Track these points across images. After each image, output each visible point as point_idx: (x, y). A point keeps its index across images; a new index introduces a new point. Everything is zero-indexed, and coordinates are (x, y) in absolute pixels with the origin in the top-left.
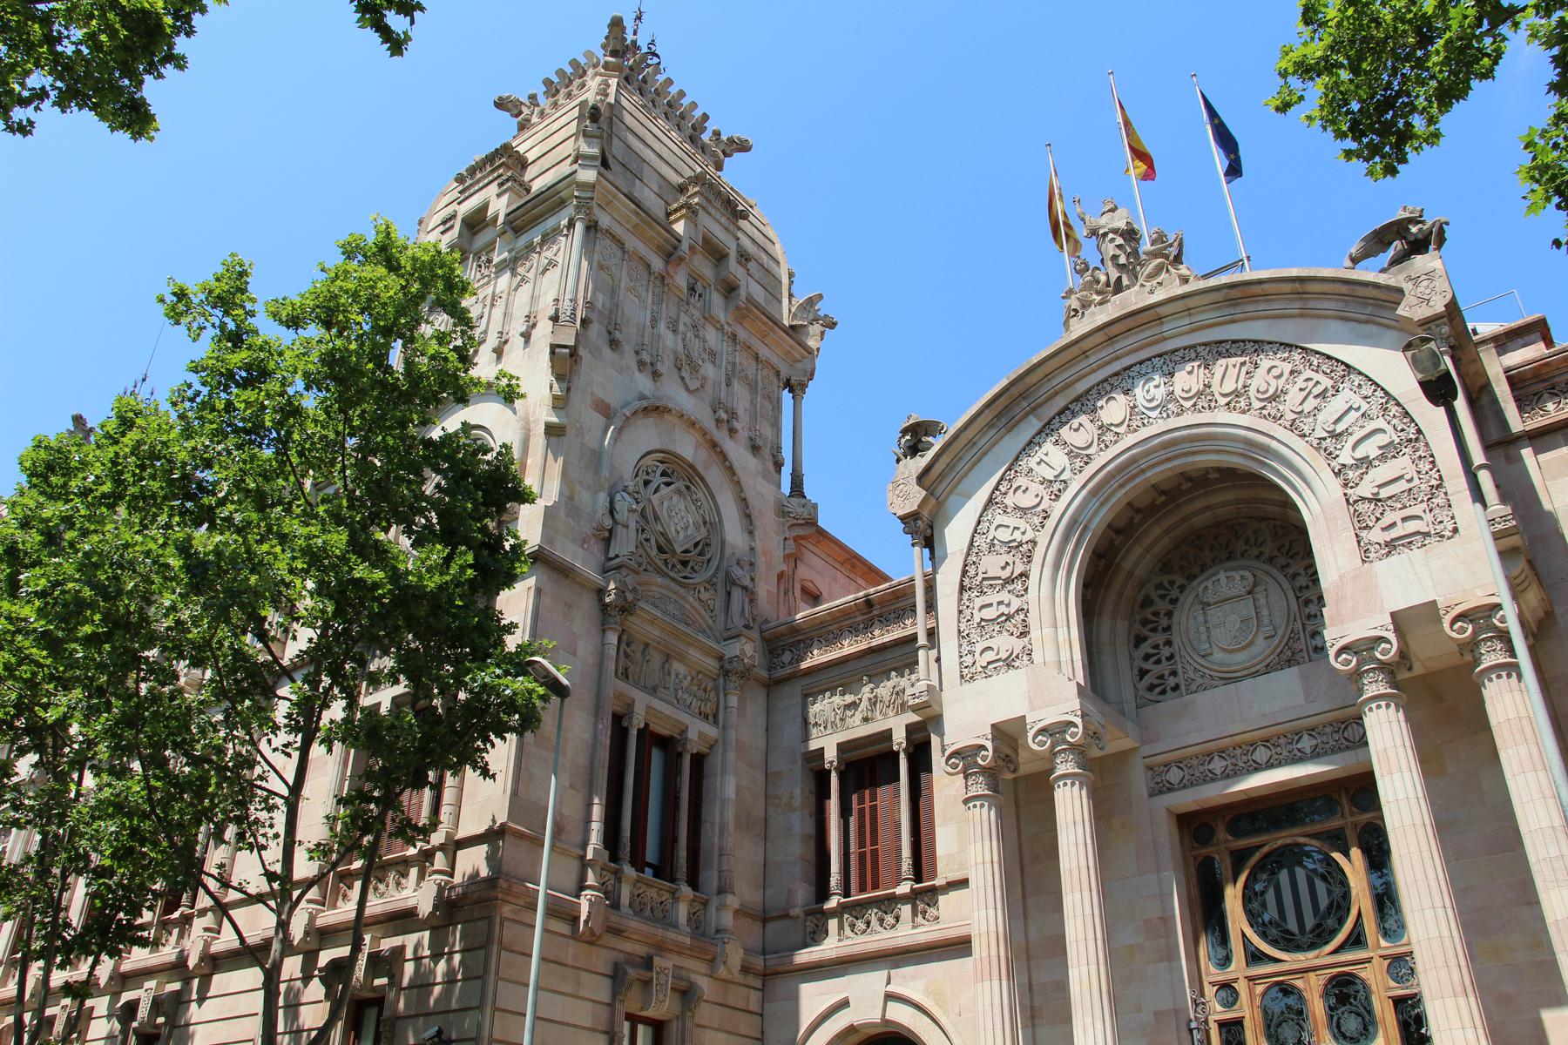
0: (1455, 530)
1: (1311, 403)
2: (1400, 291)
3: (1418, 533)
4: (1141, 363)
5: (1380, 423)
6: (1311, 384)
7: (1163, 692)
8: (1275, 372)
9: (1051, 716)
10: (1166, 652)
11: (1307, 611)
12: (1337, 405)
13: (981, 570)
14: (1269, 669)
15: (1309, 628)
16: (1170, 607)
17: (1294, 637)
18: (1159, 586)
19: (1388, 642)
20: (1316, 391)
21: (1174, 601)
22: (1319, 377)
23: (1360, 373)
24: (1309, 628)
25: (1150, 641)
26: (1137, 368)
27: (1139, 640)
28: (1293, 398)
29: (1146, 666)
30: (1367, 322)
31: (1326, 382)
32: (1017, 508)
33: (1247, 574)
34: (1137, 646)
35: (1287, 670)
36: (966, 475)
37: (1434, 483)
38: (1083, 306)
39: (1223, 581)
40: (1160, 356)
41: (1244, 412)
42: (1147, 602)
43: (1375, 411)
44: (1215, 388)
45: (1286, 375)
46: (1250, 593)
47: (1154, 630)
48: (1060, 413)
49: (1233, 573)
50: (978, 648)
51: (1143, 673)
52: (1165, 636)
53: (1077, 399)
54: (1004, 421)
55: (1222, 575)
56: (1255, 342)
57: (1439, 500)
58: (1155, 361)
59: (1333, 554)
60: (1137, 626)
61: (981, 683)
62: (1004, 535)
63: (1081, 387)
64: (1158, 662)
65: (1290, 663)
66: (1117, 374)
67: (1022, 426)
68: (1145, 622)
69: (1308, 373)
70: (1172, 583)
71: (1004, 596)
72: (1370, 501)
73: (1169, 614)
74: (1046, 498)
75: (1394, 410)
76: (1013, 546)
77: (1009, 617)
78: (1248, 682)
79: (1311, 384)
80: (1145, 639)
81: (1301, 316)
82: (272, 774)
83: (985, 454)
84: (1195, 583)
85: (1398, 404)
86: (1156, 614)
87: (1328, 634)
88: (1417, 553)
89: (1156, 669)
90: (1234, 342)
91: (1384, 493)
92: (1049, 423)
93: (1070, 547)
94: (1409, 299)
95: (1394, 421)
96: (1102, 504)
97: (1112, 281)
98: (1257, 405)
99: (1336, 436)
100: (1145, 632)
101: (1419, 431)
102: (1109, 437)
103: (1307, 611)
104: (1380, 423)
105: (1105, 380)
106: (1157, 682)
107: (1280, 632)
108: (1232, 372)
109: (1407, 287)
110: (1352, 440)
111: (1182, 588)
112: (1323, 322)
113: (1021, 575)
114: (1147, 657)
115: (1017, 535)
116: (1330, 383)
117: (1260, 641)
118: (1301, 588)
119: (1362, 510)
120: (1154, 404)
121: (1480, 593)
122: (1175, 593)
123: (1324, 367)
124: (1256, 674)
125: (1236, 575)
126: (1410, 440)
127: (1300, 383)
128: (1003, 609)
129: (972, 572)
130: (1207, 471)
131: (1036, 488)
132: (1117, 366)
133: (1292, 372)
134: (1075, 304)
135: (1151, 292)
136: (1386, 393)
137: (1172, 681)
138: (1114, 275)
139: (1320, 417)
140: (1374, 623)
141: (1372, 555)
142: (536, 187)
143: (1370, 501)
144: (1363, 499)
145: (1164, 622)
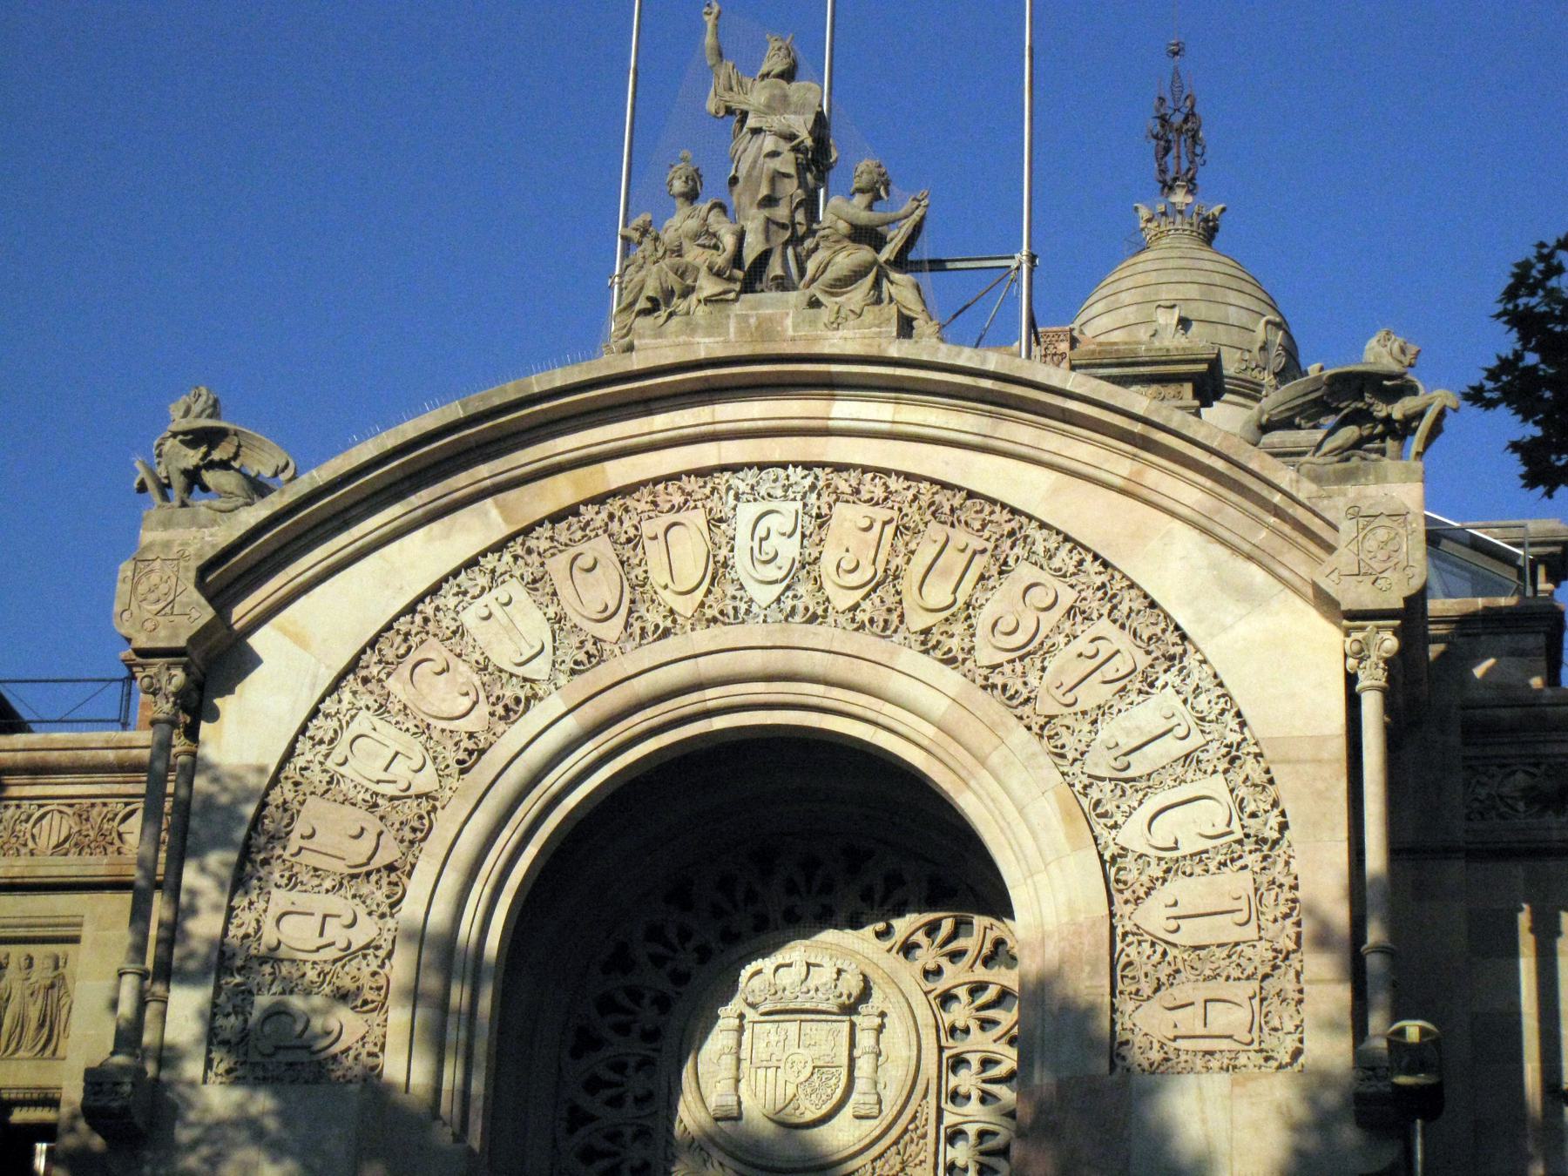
1: (1090, 696)
4: (762, 466)
8: (1040, 597)
11: (953, 1081)
12: (1147, 715)
15: (949, 1119)
16: (667, 987)
20: (1109, 671)
22: (1122, 640)
24: (949, 1119)
27: (586, 1042)
28: (1064, 663)
29: (586, 1102)
30: (1250, 558)
34: (576, 1054)
40: (808, 466)
44: (909, 584)
47: (622, 1029)
48: (556, 518)
51: (578, 1118)
63: (618, 473)
64: (616, 1102)
66: (703, 473)
68: (607, 1005)
69: (1104, 626)
70: (685, 935)
73: (663, 1003)
80: (597, 1044)
86: (635, 995)
89: (609, 1117)
90: (971, 495)
92: (527, 531)
93: (508, 837)
97: (749, 256)
99: (1124, 782)
103: (953, 1081)
104: (1217, 786)
105: (676, 477)
108: (954, 560)
113: (391, 868)
114: (593, 1085)
116: (1143, 661)
118: (953, 1031)
120: (772, 572)
123: (1135, 622)
127: (1082, 644)
133: (1070, 612)
135: (836, 324)
139: (1109, 730)
142: (237, 627)
145: (648, 1015)
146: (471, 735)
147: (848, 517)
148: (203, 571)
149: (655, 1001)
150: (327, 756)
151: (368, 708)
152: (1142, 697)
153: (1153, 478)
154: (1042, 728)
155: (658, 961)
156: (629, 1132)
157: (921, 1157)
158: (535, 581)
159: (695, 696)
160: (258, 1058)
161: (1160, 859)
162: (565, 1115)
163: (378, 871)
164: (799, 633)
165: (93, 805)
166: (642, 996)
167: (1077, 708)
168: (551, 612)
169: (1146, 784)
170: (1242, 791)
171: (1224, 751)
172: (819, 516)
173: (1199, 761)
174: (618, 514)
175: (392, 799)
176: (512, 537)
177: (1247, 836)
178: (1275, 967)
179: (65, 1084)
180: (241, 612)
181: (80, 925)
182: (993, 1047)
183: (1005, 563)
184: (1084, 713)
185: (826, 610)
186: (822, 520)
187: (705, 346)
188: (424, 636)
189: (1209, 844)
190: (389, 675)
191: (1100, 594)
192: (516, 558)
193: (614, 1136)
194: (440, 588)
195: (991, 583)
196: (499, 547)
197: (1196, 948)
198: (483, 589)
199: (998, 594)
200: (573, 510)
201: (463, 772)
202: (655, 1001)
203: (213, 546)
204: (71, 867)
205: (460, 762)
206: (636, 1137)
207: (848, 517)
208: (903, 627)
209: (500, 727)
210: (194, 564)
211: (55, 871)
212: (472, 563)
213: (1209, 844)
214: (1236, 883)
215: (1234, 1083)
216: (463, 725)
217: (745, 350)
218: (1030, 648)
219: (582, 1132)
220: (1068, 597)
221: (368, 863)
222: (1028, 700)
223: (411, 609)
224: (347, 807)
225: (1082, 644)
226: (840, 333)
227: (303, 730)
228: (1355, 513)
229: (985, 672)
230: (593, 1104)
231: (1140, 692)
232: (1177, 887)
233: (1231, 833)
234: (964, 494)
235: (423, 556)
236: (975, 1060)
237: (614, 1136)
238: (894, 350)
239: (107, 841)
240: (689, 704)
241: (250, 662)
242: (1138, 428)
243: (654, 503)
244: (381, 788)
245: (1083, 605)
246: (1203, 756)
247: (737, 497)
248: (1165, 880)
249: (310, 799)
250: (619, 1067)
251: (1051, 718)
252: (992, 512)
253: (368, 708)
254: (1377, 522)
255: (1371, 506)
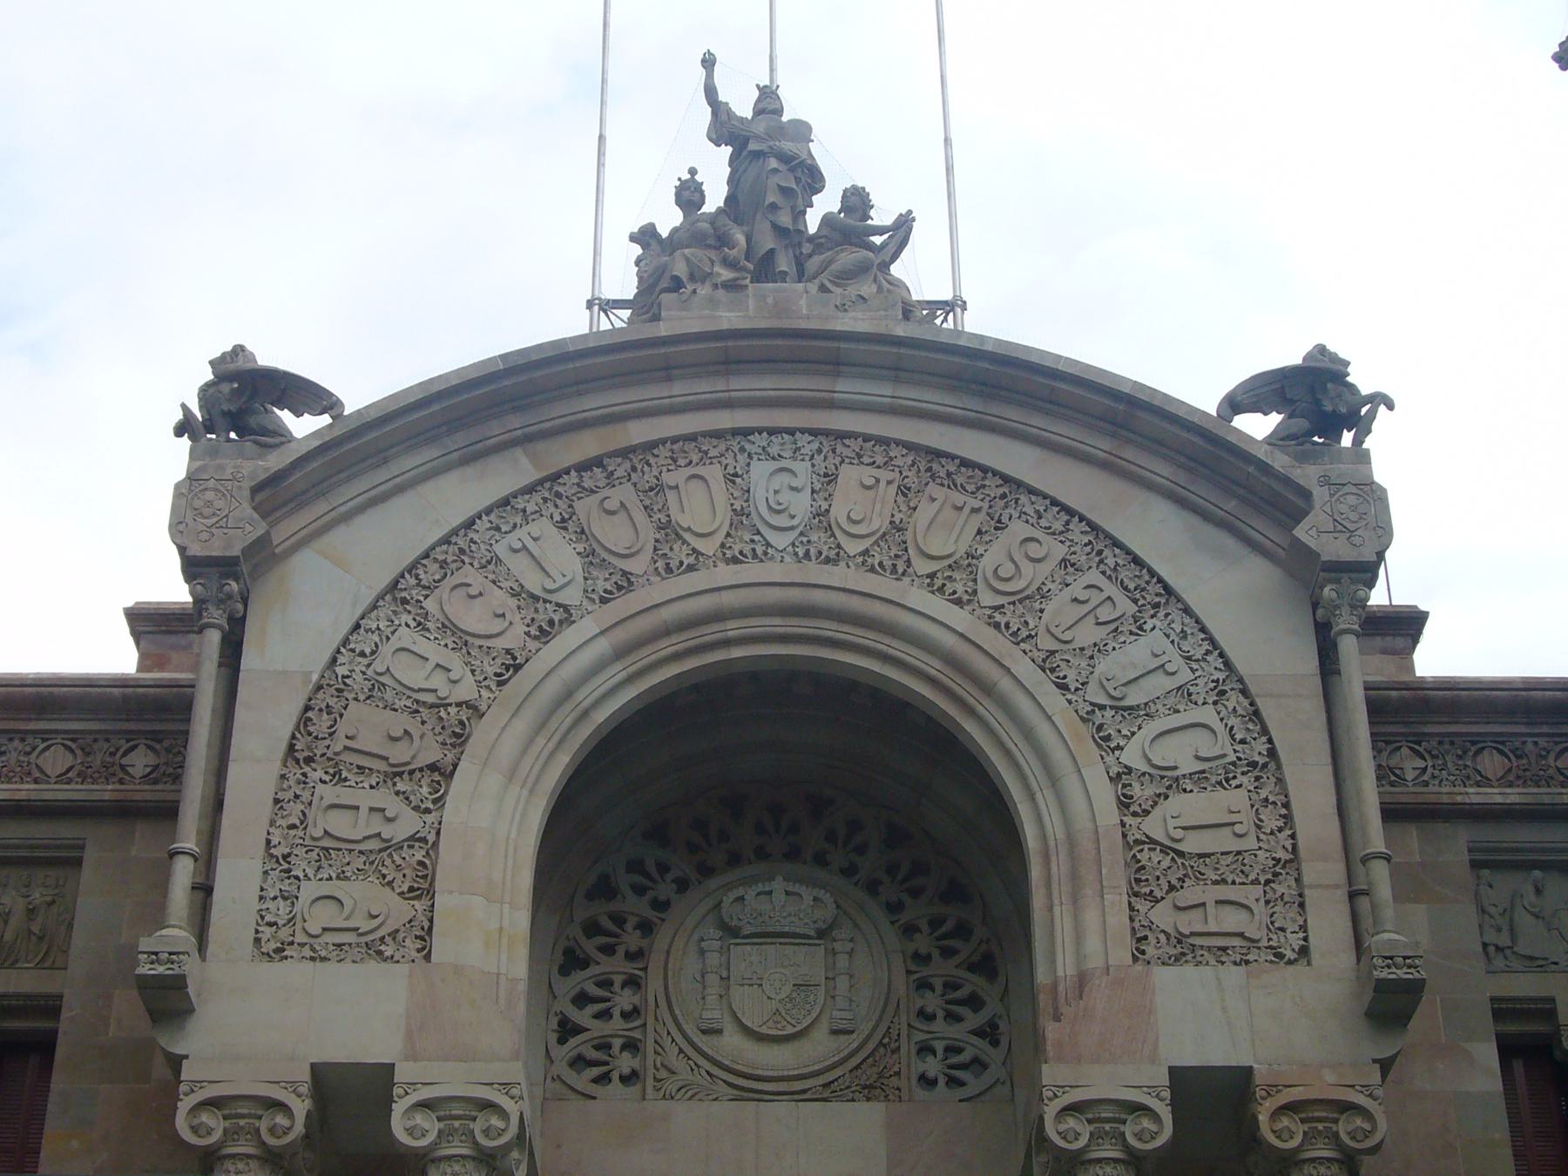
0: (1304, 951)
1: (1087, 634)
2: (1306, 495)
3: (1241, 935)
4: (773, 432)
5: (1207, 715)
6: (1096, 597)
7: (603, 1079)
9: (453, 1081)
10: (625, 999)
12: (1138, 653)
13: (343, 728)
14: (829, 1092)
16: (650, 914)
17: (888, 1045)
18: (635, 866)
19: (1156, 1117)
20: (1105, 613)
21: (661, 906)
22: (1111, 590)
23: (1187, 610)
25: (593, 970)
26: (760, 440)
28: (1059, 610)
31: (1125, 606)
32: (448, 626)
33: (827, 898)
35: (863, 1107)
36: (347, 517)
37: (1281, 854)
38: (692, 278)
39: (779, 897)
40: (814, 433)
41: (958, 602)
42: (604, 889)
43: (1201, 690)
45: (1051, 564)
46: (821, 934)
47: (609, 950)
48: (583, 467)
49: (802, 889)
50: (308, 891)
51: (567, 1030)
52: (631, 968)
53: (625, 453)
54: (460, 439)
55: (778, 885)
56: (1006, 479)
57: (1285, 887)
58: (803, 439)
59: (1078, 931)
60: (576, 931)
61: (296, 971)
62: (414, 675)
63: (639, 432)
64: (605, 1015)
65: (870, 1091)
66: (718, 435)
67: (495, 462)
68: (592, 929)
69: (1094, 576)
70: (663, 868)
71: (384, 798)
72: (1165, 850)
73: (646, 928)
74: (520, 629)
75: (1234, 699)
76: (425, 706)
77: (389, 847)
78: (781, 1108)
79: (1096, 597)
80: (584, 963)
81: (1105, 466)
82: (1008, 1084)
83: (400, 490)
84: (713, 883)
85: (1244, 692)
87: (1050, 1074)
88: (1233, 975)
89: (598, 1029)
91: (1192, 844)
92: (555, 477)
94: (1317, 517)
95: (1232, 721)
96: (630, 680)
98: (987, 598)
100: (590, 946)
101: (1272, 753)
102: (680, 554)
105: (692, 438)
106: (593, 1055)
107: (866, 1028)
109: (1319, 494)
110: (1152, 728)
111: (683, 885)
112: (1142, 495)
113: (433, 767)
114: (582, 1000)
115: (438, 681)
117: (821, 1034)
119: (1154, 870)
121: (1330, 1077)
122: (665, 890)
123: (1124, 574)
124: (800, 1096)
125: (807, 894)
126: (1253, 765)
127: (1076, 590)
128: (377, 825)
129: (321, 724)
130: (853, 686)
131: (802, 505)
132: (743, 419)
133: (1064, 563)
134: (680, 269)
135: (842, 308)
136: (1228, 664)
137: (626, 1062)
138: (767, 242)
139: (1103, 666)
140: (1137, 1079)
141: (1151, 951)
143: (1165, 850)
144: (1152, 841)
146: (508, 651)
147: (851, 475)
148: (255, 490)
149: (638, 927)
150: (369, 665)
151: (407, 625)
152: (1133, 638)
153: (1129, 453)
154: (1044, 661)
155: (640, 891)
156: (617, 1043)
157: (896, 1069)
158: (563, 520)
159: (716, 627)
160: (305, 939)
161: (1162, 777)
162: (556, 1027)
163: (421, 770)
164: (815, 572)
165: (95, 740)
166: (625, 921)
167: (1076, 645)
168: (580, 548)
169: (1142, 712)
170: (1232, 721)
171: (1212, 685)
172: (826, 475)
173: (1190, 695)
174: (639, 467)
175: (432, 706)
176: (541, 482)
177: (1239, 759)
178: (1276, 875)
179: (66, 992)
180: (283, 532)
181: (82, 848)
182: (956, 972)
183: (999, 521)
184: (1082, 649)
185: (838, 554)
186: (830, 478)
187: (729, 318)
188: (459, 564)
189: (1205, 766)
190: (426, 597)
191: (1088, 549)
192: (545, 500)
193: (604, 1046)
194: (473, 523)
195: (986, 538)
196: (530, 490)
197: (1200, 856)
198: (515, 526)
199: (996, 546)
200: (598, 462)
201: (500, 684)
202: (638, 927)
203: (266, 470)
204: (76, 792)
205: (497, 675)
206: (624, 1048)
207: (851, 475)
208: (910, 570)
209: (532, 645)
210: (247, 485)
211: (61, 796)
212: (505, 502)
213: (1205, 766)
214: (1237, 799)
215: (1249, 974)
216: (500, 644)
217: (763, 324)
218: (1028, 592)
219: (573, 1042)
220: (1060, 551)
221: (408, 763)
222: (1030, 636)
223: (446, 540)
224: (388, 711)
225: (1076, 590)
226: (850, 314)
227: (346, 642)
228: (1325, 481)
229: (989, 612)
230: (583, 1017)
231: (1131, 633)
232: (1176, 803)
233: (1224, 756)
234: (957, 461)
235: (459, 496)
236: (938, 983)
237: (604, 1046)
238: (900, 331)
239: (114, 771)
240: (710, 633)
241: (802, 131)
242: (518, 816)
243: (675, 460)
244: (422, 697)
245: (1073, 558)
246: (1192, 689)
247: (750, 456)
248: (1167, 797)
249: (352, 704)
250: (606, 984)
251: (1053, 653)
252: (984, 479)
253: (407, 625)
254: (1346, 489)
255: (1339, 476)
